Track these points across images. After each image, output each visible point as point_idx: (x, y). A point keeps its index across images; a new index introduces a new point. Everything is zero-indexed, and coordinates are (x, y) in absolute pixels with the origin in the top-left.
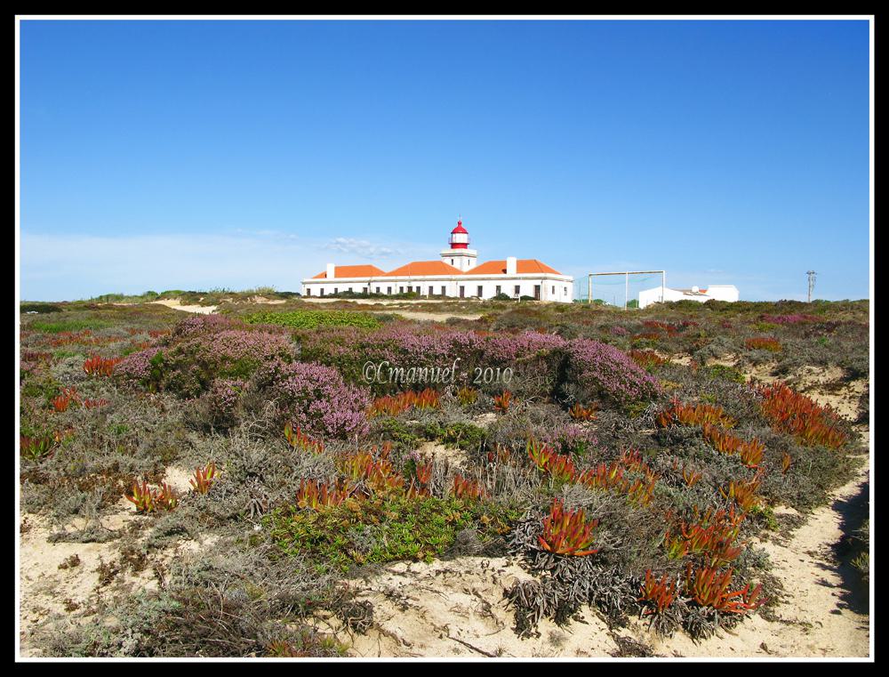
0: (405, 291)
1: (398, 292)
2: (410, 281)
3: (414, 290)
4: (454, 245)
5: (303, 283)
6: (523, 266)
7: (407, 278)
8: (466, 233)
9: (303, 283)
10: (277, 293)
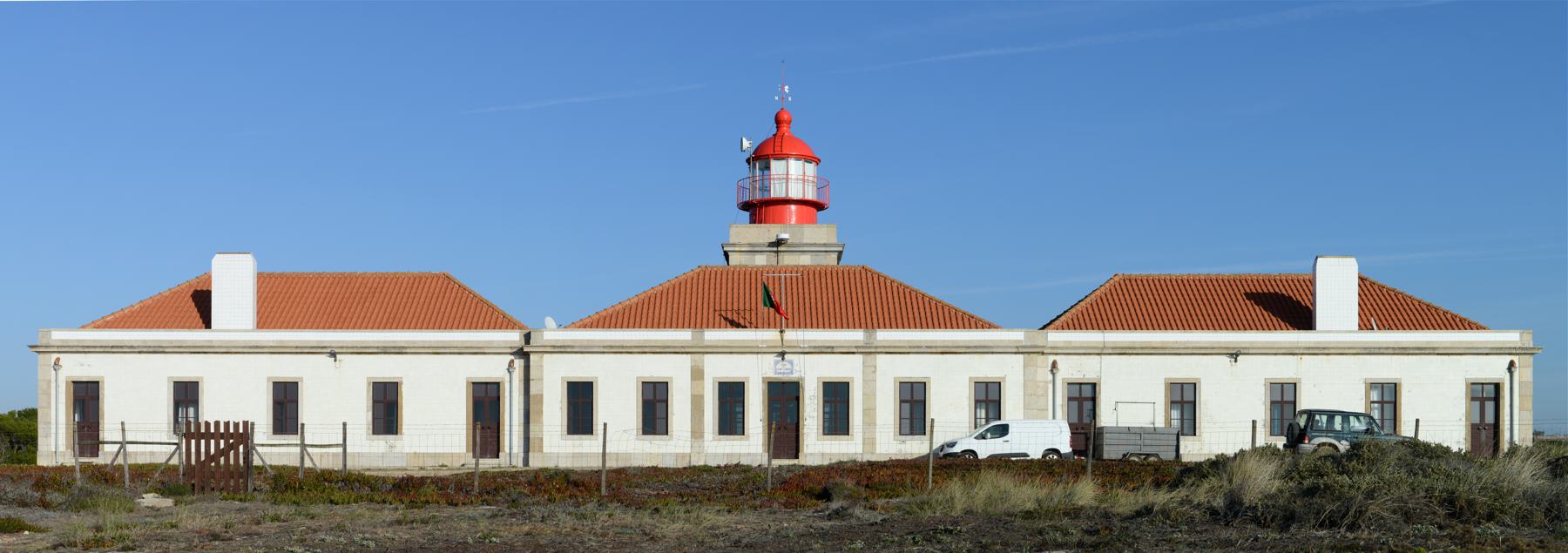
4: (759, 209)
6: (1382, 306)
8: (817, 161)
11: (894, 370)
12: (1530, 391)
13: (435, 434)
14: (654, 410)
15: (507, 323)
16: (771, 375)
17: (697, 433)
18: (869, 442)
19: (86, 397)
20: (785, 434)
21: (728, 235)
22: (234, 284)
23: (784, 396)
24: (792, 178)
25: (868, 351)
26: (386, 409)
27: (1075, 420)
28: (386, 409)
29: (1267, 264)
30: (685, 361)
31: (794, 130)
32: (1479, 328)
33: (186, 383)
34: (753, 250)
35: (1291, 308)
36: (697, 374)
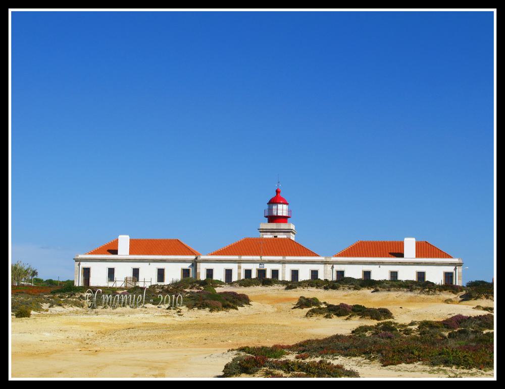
0: (254, 275)
1: (243, 277)
2: (262, 262)
3: (269, 275)
4: (273, 219)
5: (77, 260)
6: (424, 249)
7: (257, 258)
8: (287, 204)
9: (77, 260)
10: (50, 282)
12: (461, 275)
15: (192, 253)
16: (258, 268)
21: (259, 226)
22: (410, 247)
24: (281, 210)
25: (239, 262)
30: (322, 266)
31: (281, 195)
32: (317, 256)
33: (314, 271)
36: (239, 268)
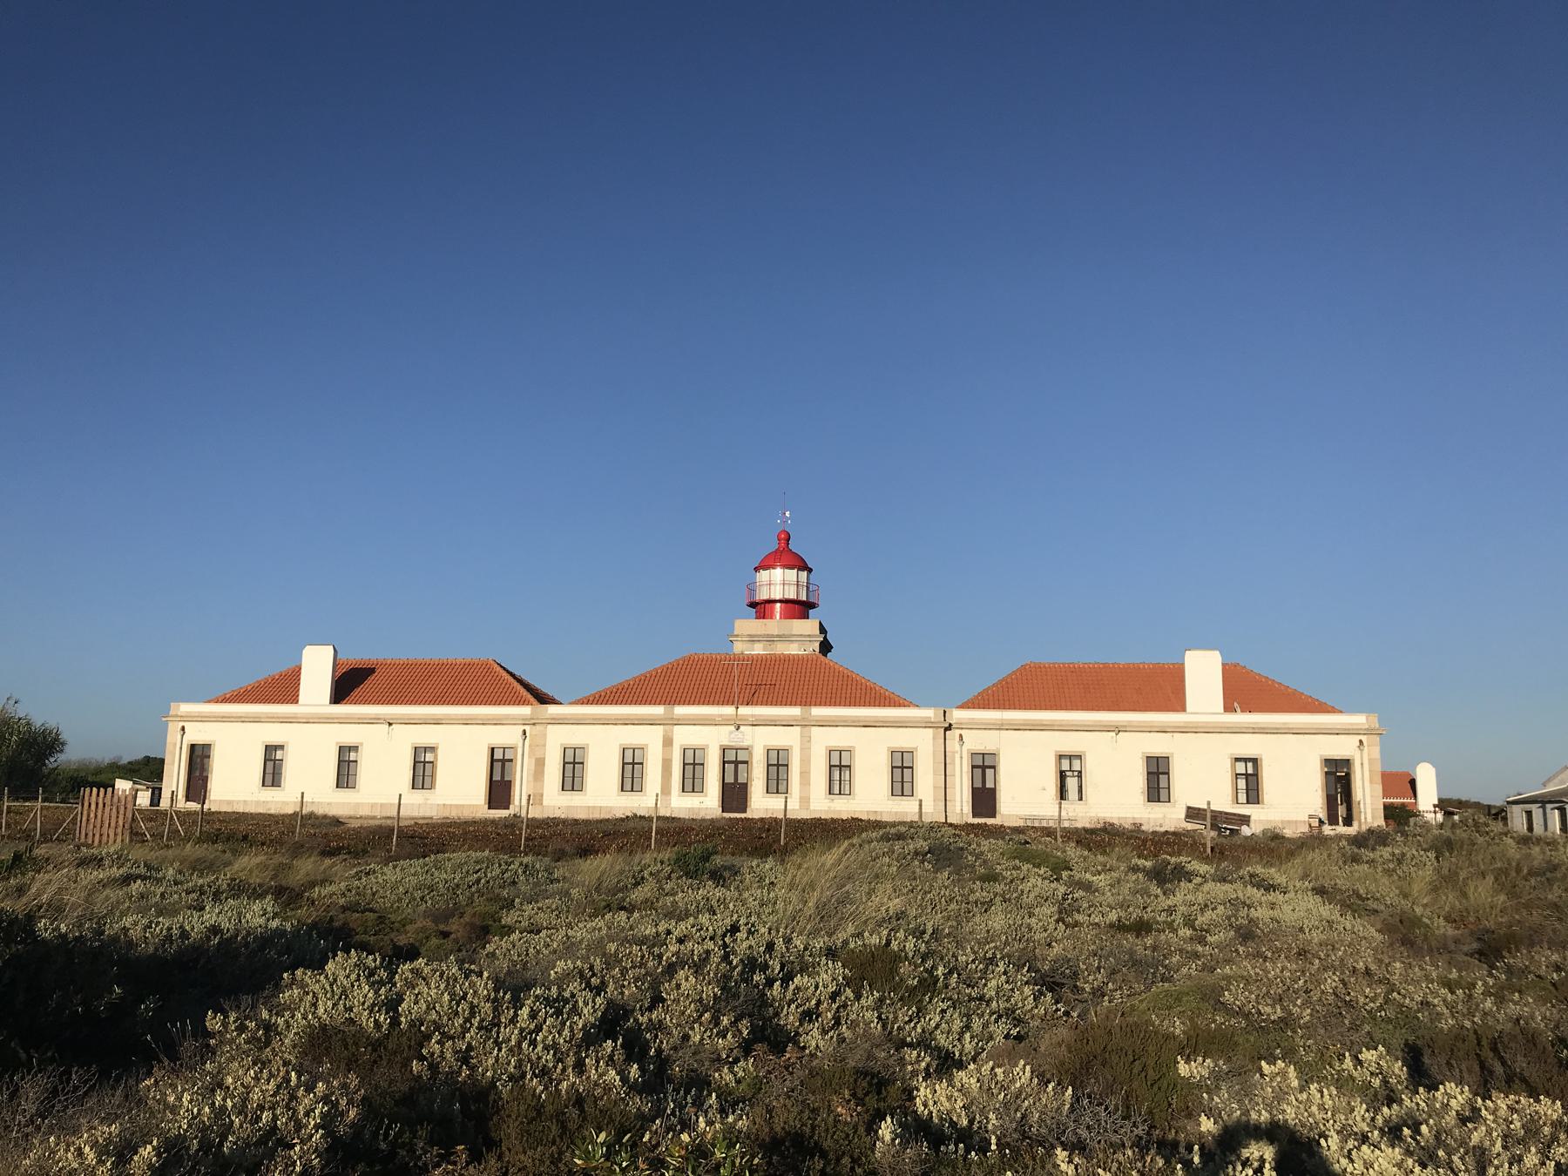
6: (1244, 691)
11: (557, 739)
13: (460, 792)
14: (631, 771)
17: (666, 790)
18: (805, 800)
19: (199, 758)
20: (734, 795)
23: (734, 761)
25: (805, 724)
26: (423, 770)
27: (978, 784)
28: (423, 770)
29: (1129, 650)
30: (659, 731)
34: (753, 639)
35: (1162, 689)
36: (668, 742)
